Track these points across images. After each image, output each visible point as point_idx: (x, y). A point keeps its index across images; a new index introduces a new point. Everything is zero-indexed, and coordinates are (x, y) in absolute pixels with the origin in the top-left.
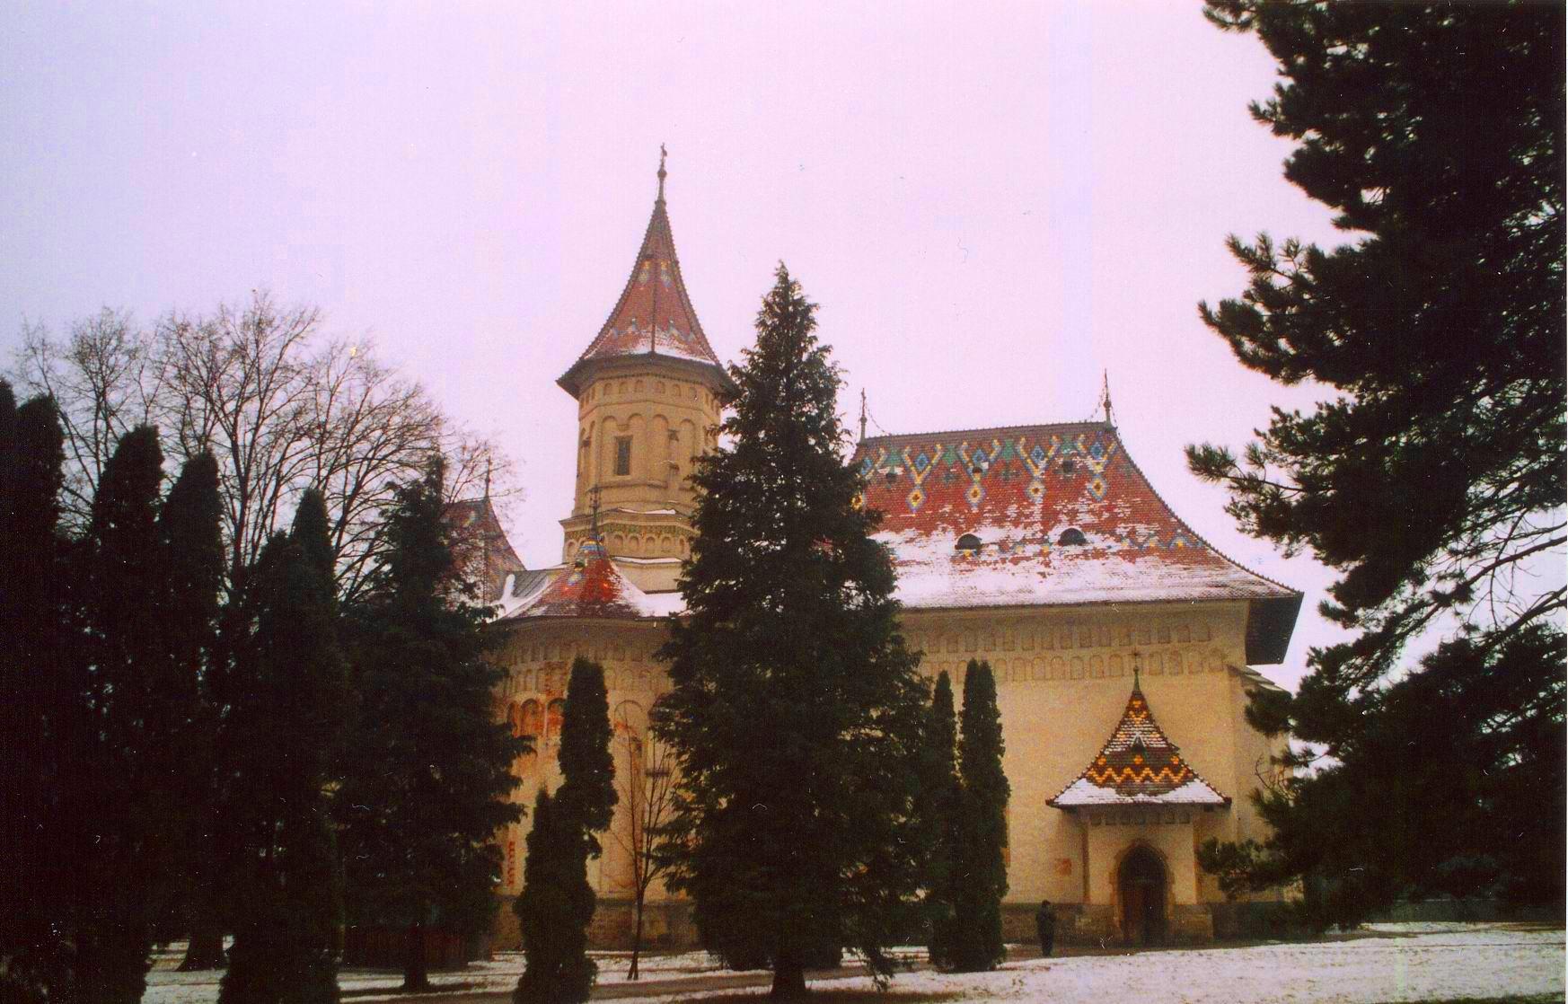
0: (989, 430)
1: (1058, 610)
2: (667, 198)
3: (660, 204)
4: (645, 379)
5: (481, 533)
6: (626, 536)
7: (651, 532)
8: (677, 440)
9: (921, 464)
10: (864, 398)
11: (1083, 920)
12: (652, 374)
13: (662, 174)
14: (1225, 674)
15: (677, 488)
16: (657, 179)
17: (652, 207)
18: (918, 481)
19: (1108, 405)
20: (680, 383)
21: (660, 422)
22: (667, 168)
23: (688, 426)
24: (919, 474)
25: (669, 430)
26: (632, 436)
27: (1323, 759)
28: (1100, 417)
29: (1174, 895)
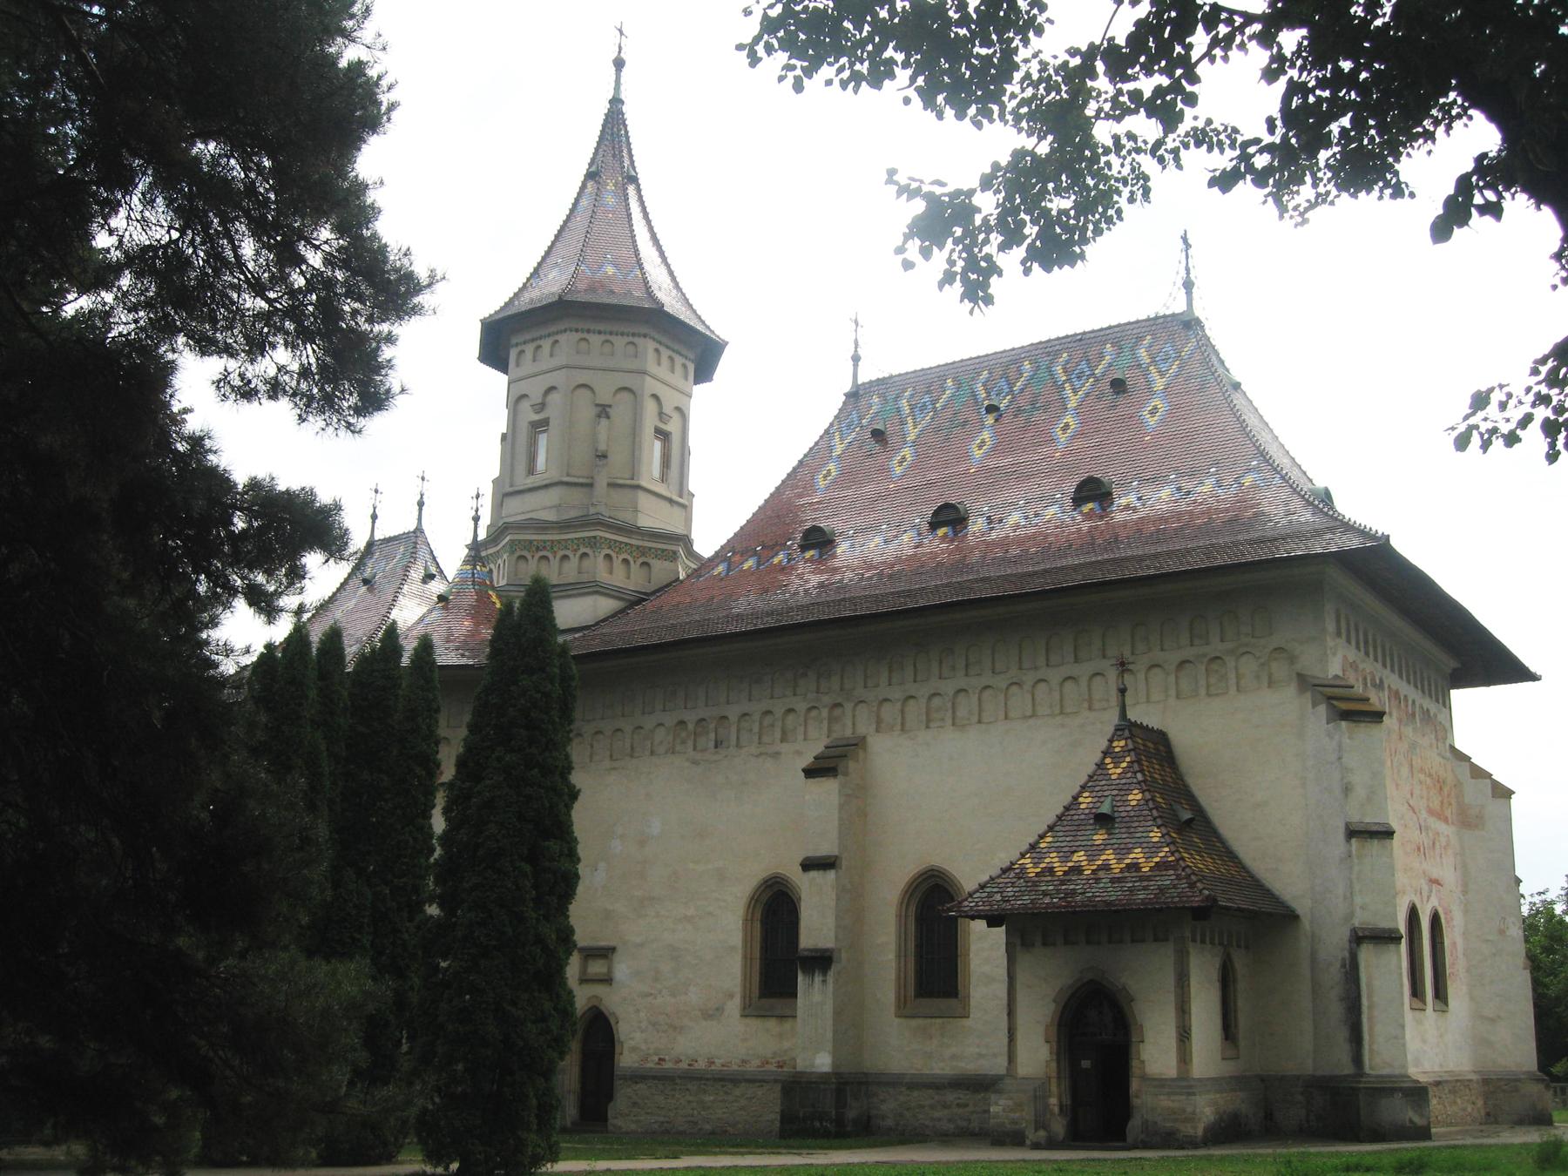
1: (581, 634)
3: (616, 102)
4: (562, 338)
6: (533, 557)
7: (566, 548)
8: (608, 417)
9: (1079, 378)
10: (1188, 246)
11: (1002, 1102)
13: (619, 64)
14: (1291, 691)
15: (605, 484)
17: (604, 107)
18: (1072, 404)
19: (1188, 285)
23: (626, 396)
24: (1075, 391)
25: (597, 405)
26: (548, 418)
28: (1179, 306)
29: (1143, 1062)
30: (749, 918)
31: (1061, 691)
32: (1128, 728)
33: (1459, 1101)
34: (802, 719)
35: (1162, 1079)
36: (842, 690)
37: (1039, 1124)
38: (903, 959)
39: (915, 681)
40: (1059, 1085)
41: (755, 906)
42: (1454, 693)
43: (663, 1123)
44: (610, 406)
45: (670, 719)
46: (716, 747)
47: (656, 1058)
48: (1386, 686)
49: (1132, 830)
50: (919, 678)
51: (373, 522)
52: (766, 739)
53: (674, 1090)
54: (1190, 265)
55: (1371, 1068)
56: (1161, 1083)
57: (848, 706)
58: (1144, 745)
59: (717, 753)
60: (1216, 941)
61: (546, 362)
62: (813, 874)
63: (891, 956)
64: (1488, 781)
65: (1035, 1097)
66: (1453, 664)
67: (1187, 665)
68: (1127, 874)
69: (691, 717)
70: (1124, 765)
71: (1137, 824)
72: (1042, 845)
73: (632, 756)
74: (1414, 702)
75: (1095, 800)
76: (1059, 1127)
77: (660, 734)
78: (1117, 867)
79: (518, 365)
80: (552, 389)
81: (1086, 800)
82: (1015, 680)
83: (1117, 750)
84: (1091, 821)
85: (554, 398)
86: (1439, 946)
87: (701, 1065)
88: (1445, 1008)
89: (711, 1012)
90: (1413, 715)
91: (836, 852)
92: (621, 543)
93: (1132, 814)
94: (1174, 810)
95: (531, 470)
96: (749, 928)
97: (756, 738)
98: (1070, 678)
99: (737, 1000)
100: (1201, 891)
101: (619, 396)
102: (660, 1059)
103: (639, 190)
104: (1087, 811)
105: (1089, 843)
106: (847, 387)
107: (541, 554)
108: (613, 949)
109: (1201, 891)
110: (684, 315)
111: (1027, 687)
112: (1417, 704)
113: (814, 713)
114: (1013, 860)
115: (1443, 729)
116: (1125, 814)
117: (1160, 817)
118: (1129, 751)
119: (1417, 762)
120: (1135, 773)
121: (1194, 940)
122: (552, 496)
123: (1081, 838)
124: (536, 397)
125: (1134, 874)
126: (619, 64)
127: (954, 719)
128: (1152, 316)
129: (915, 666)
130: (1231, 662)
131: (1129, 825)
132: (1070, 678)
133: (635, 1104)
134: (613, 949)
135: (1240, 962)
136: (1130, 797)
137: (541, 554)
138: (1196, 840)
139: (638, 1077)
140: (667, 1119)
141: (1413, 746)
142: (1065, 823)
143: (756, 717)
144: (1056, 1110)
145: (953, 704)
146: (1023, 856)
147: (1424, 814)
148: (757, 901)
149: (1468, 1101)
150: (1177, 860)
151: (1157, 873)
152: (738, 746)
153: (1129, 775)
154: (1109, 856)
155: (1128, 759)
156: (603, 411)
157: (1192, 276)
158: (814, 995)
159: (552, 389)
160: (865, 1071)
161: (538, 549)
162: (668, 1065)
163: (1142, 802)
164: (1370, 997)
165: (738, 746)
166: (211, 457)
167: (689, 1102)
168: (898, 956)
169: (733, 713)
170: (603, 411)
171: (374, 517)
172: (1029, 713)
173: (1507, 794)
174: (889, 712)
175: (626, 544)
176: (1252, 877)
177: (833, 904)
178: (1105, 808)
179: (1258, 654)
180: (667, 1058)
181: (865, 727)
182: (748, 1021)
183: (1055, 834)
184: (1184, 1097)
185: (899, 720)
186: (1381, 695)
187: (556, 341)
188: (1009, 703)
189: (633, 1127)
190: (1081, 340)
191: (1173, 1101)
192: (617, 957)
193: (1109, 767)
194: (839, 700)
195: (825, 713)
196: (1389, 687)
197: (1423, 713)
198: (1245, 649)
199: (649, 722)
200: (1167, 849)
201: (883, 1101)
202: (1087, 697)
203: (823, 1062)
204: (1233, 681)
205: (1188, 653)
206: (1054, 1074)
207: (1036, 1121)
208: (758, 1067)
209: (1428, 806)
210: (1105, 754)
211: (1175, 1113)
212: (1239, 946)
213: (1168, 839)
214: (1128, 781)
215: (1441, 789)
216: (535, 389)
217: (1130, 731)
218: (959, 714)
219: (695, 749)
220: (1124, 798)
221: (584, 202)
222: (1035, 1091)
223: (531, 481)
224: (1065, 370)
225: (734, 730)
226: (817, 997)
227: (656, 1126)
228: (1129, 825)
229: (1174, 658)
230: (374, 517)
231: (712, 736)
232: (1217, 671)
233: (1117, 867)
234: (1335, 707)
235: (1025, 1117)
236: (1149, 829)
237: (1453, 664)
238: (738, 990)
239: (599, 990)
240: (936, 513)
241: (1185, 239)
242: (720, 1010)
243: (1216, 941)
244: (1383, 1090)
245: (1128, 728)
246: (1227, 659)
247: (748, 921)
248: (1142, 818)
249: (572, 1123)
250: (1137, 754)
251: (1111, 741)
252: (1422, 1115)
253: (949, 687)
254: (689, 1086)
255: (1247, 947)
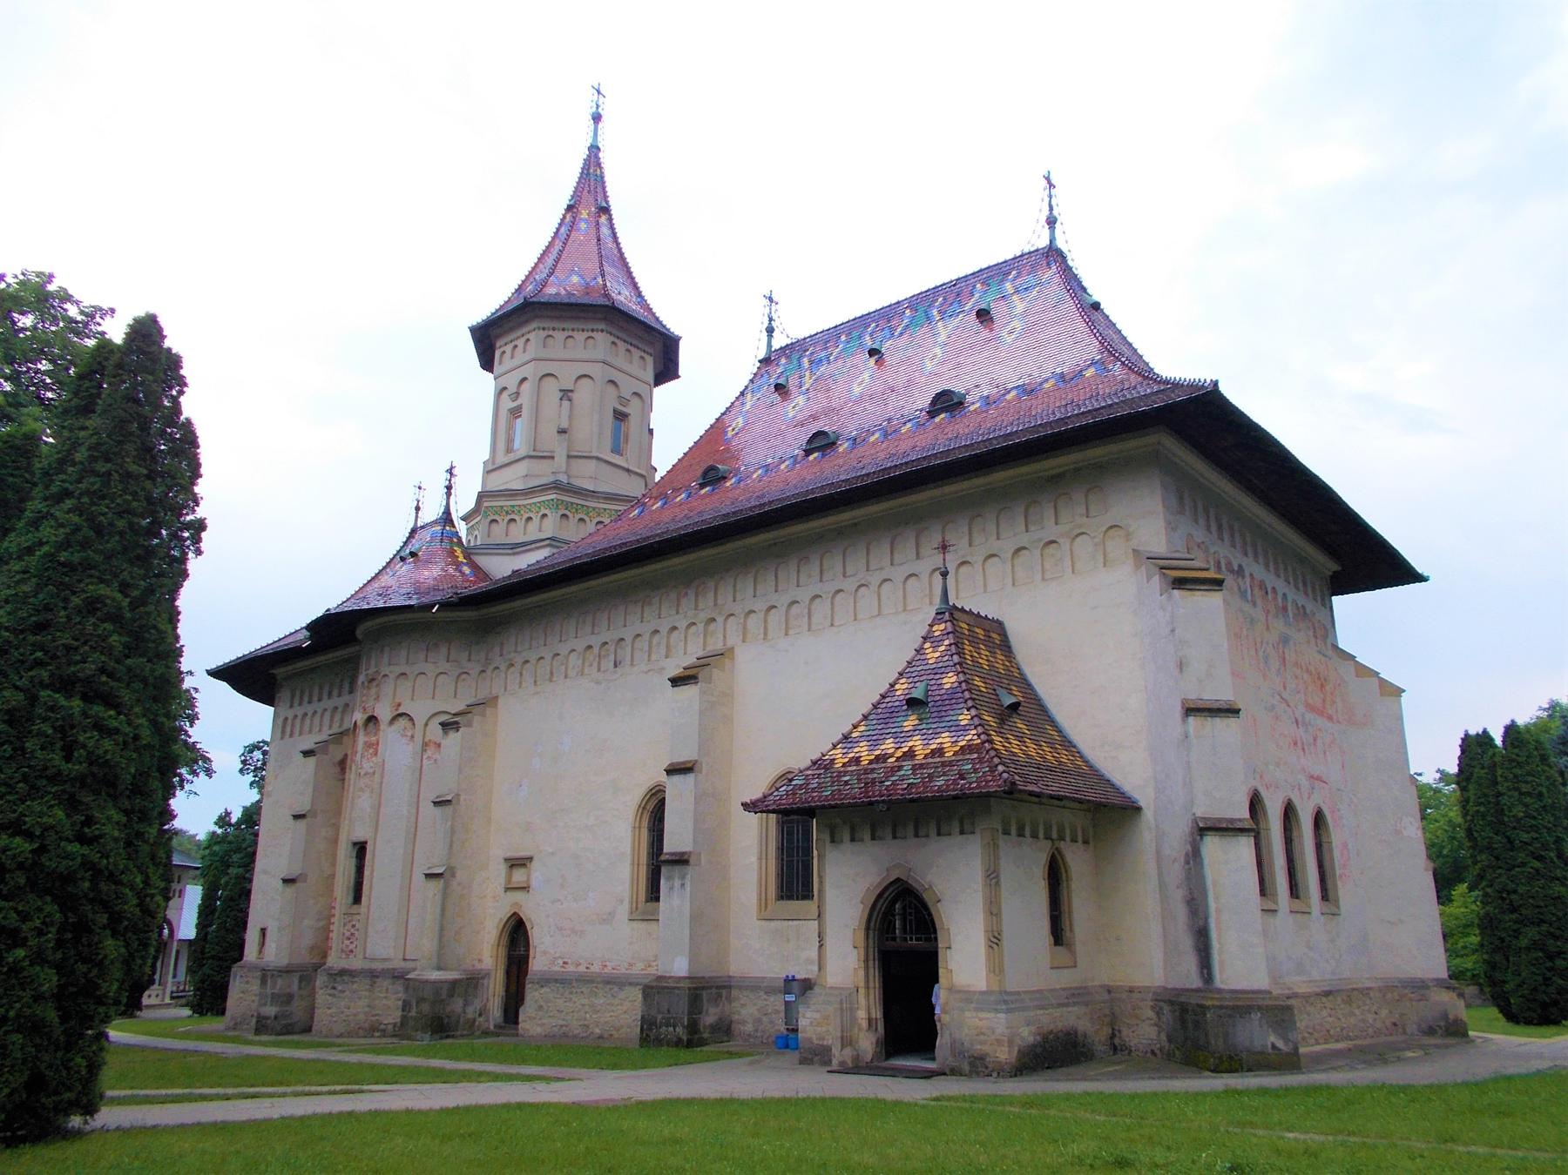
3: (594, 150)
4: (531, 336)
13: (597, 118)
17: (584, 153)
19: (1051, 222)
25: (561, 390)
30: (637, 825)
31: (904, 589)
32: (950, 612)
33: (1357, 1012)
34: (683, 635)
35: (969, 992)
36: (715, 605)
37: (846, 1041)
38: (764, 861)
39: (776, 591)
40: (867, 995)
41: (642, 813)
42: (1334, 598)
43: (562, 1026)
44: (572, 391)
45: (580, 645)
46: (616, 666)
47: (561, 962)
48: (1247, 574)
49: (943, 714)
50: (780, 589)
51: (417, 513)
52: (654, 657)
53: (571, 993)
54: (1053, 203)
55: (1222, 982)
56: (967, 996)
57: (720, 620)
58: (969, 630)
59: (615, 672)
60: (1041, 835)
61: (520, 357)
62: (677, 779)
63: (754, 859)
64: (1375, 680)
65: (842, 1009)
66: (1334, 567)
67: (1024, 552)
68: (930, 760)
69: (596, 641)
70: (943, 648)
71: (948, 707)
72: (854, 735)
73: (551, 681)
74: (1284, 595)
75: (911, 686)
76: (867, 1043)
77: (574, 660)
78: (921, 752)
79: (500, 363)
80: (524, 379)
81: (901, 687)
82: (863, 582)
83: (936, 634)
84: (905, 707)
85: (526, 385)
86: (1325, 845)
87: (596, 968)
88: (1334, 910)
89: (605, 917)
90: (1285, 609)
91: (694, 756)
92: (577, 504)
93: (945, 697)
94: (997, 695)
95: (509, 450)
96: (637, 833)
97: (646, 656)
98: (911, 575)
99: (626, 906)
100: (1000, 775)
101: (579, 382)
102: (564, 963)
103: (610, 219)
104: (902, 698)
105: (899, 730)
106: (762, 354)
107: (509, 517)
108: (531, 859)
109: (1000, 775)
110: (633, 307)
111: (874, 588)
112: (1290, 599)
113: (693, 629)
114: (824, 751)
115: (1327, 628)
116: (939, 698)
117: (971, 698)
118: (948, 633)
119: (1290, 656)
120: (952, 655)
121: (1006, 832)
122: (521, 469)
123: (892, 726)
124: (512, 388)
125: (938, 760)
126: (597, 118)
127: (810, 625)
128: (1019, 254)
129: (776, 577)
130: (1065, 543)
131: (940, 708)
132: (911, 575)
133: (541, 1007)
134: (531, 859)
135: (1077, 860)
136: (944, 681)
137: (509, 517)
138: (986, 718)
139: (546, 980)
140: (564, 1023)
141: (1285, 640)
142: (880, 711)
143: (647, 636)
144: (864, 1024)
145: (809, 610)
146: (834, 746)
147: (1301, 708)
148: (644, 808)
149: (1369, 1011)
150: (983, 743)
151: (961, 757)
152: (632, 665)
153: (946, 658)
154: (916, 742)
155: (947, 642)
156: (566, 394)
157: (1055, 212)
158: (676, 898)
159: (524, 379)
160: (731, 974)
161: (507, 512)
162: (570, 968)
163: (956, 684)
164: (1217, 898)
165: (632, 665)
166: (657, 599)
167: (583, 1005)
168: (760, 859)
169: (628, 634)
170: (566, 394)
171: (418, 509)
172: (876, 613)
173: (1399, 692)
174: (754, 623)
175: (583, 506)
176: (1091, 767)
177: (692, 807)
178: (918, 693)
179: (1092, 535)
180: (569, 961)
181: (733, 639)
182: (636, 925)
183: (868, 722)
184: (992, 1015)
185: (762, 631)
186: (1241, 583)
187: (528, 340)
188: (858, 604)
189: (539, 1030)
190: (954, 285)
191: (981, 1020)
192: (535, 865)
193: (927, 651)
194: (713, 615)
195: (701, 626)
196: (1251, 575)
197: (1298, 608)
198: (1079, 531)
199: (563, 649)
200: (974, 732)
201: (743, 1005)
202: (927, 592)
203: (680, 967)
204: (1068, 563)
205: (1024, 539)
206: (862, 984)
207: (842, 1038)
208: (642, 970)
209: (1306, 701)
210: (925, 639)
211: (983, 1034)
212: (1074, 840)
213: (976, 721)
214: (946, 664)
215: (1322, 686)
216: (511, 381)
217: (951, 614)
218: (814, 620)
219: (599, 670)
220: (939, 682)
221: (563, 230)
222: (841, 1002)
223: (512, 457)
224: (939, 312)
225: (629, 649)
226: (676, 902)
227: (556, 1029)
228: (940, 708)
229: (1007, 546)
230: (418, 509)
231: (612, 657)
232: (1052, 555)
233: (921, 752)
234: (1164, 574)
235: (831, 1036)
236: (959, 712)
237: (1334, 567)
238: (626, 895)
239: (518, 896)
240: (810, 441)
241: (1048, 179)
242: (612, 914)
243: (1041, 835)
244: (1235, 1008)
245: (950, 612)
246: (1061, 541)
247: (637, 828)
248: (954, 701)
249: (495, 1026)
250: (955, 638)
251: (931, 626)
252: (1286, 1040)
253: (804, 594)
254: (584, 989)
255: (1086, 842)
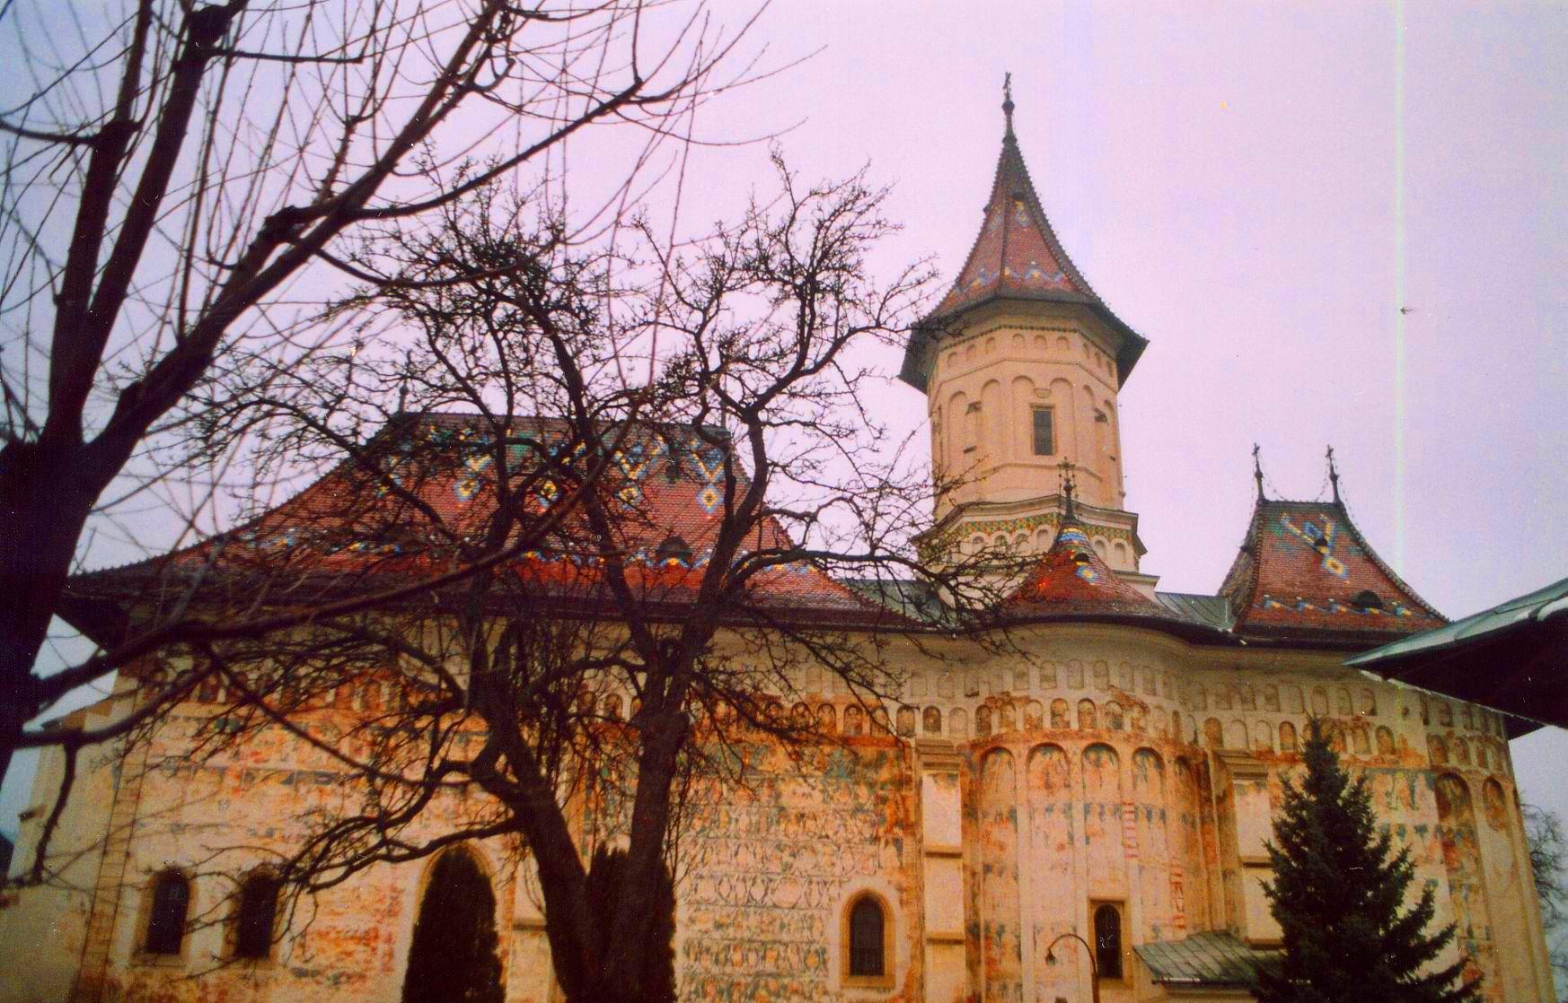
0: (1294, 503)
2: (1017, 132)
3: (1010, 139)
4: (997, 334)
5: (539, 505)
7: (999, 529)
12: (1005, 327)
16: (1002, 114)
17: (999, 147)
20: (1067, 335)
21: (1022, 385)
22: (1014, 99)
27: (217, 44)
